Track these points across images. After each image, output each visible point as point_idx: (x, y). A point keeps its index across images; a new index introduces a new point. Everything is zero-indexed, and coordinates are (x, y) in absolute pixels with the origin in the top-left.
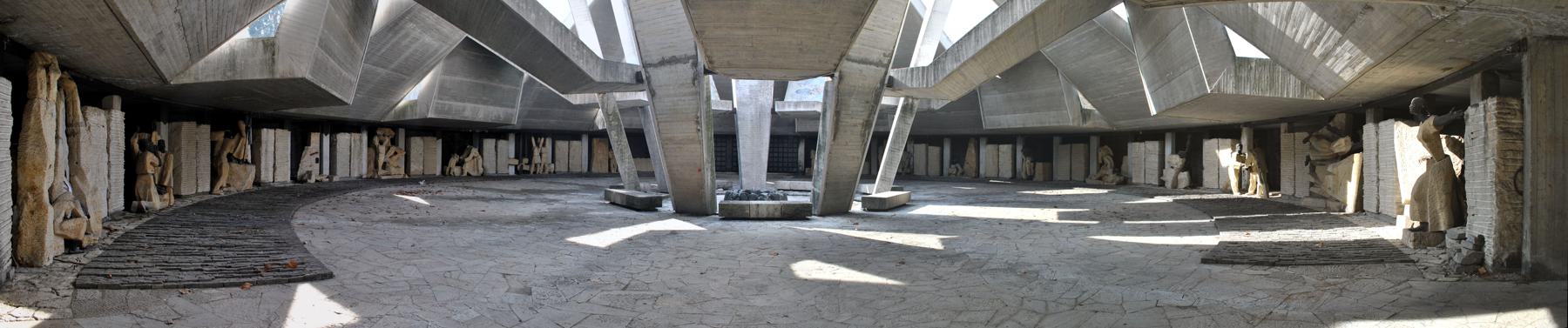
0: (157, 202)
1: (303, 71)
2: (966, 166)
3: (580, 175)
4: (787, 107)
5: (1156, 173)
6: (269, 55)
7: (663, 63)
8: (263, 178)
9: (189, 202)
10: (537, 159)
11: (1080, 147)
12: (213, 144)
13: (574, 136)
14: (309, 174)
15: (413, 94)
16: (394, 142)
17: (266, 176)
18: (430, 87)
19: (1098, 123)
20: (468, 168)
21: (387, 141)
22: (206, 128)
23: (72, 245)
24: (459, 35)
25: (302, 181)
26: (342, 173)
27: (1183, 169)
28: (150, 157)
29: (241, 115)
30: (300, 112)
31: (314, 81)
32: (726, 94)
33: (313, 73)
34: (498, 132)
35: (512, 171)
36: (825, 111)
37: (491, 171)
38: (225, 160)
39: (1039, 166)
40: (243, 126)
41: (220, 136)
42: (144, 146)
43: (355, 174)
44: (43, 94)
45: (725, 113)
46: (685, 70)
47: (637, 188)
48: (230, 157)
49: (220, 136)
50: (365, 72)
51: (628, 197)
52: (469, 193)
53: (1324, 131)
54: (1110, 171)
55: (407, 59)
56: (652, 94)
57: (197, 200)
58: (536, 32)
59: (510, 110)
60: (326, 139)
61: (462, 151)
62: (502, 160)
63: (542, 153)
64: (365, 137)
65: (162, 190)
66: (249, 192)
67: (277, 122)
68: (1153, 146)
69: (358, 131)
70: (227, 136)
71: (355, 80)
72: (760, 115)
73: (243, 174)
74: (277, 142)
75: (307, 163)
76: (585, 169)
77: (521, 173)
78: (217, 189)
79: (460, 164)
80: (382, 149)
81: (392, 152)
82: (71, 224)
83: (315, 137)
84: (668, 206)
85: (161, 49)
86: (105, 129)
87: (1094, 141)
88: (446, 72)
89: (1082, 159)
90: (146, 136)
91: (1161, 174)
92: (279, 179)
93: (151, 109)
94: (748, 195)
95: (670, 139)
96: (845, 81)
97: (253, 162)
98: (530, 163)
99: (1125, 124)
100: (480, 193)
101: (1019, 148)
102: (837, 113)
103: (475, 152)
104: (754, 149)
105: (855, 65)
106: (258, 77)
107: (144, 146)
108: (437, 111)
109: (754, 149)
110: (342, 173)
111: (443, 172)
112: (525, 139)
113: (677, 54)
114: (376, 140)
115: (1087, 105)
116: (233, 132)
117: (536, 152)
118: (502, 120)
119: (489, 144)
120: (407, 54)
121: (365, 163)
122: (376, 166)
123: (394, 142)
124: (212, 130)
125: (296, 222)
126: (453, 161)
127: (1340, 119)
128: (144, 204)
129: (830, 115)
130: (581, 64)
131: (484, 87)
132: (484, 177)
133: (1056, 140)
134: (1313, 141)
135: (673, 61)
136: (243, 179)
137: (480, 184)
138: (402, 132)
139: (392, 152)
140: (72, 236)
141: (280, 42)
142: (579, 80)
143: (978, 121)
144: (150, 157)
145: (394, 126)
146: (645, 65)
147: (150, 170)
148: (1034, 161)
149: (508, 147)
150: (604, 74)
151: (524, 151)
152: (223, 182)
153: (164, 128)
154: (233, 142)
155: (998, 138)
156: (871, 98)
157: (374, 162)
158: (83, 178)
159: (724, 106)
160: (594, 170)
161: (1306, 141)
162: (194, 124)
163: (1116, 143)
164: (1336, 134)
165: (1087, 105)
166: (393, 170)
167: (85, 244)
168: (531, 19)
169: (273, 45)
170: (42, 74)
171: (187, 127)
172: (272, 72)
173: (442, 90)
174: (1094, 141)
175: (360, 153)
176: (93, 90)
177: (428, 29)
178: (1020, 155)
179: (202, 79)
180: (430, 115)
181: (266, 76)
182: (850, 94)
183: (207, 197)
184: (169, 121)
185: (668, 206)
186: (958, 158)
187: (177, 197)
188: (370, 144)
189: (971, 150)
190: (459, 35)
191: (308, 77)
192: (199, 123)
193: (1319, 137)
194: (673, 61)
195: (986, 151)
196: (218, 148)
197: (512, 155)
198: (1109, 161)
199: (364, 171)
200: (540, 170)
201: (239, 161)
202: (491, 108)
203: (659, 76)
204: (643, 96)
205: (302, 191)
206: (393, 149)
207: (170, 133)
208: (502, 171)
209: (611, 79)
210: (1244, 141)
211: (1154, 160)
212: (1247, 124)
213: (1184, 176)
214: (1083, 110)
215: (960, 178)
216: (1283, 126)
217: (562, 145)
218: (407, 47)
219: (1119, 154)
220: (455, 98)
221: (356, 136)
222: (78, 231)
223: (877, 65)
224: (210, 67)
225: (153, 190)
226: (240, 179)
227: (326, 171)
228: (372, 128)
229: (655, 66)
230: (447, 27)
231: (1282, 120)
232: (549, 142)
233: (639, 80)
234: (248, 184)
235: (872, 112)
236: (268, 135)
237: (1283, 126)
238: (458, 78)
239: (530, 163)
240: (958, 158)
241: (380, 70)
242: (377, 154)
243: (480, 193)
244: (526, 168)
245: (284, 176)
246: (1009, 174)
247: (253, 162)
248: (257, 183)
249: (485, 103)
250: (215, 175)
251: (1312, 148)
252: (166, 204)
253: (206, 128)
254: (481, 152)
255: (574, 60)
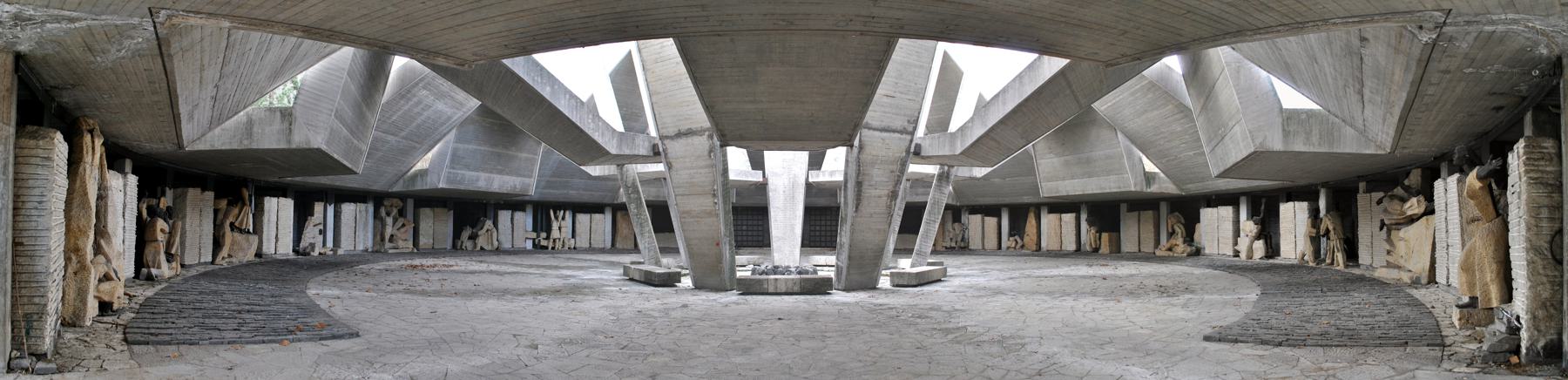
0: (165, 270)
1: (318, 141)
2: (1026, 239)
3: (603, 251)
4: (818, 177)
5: (1231, 241)
6: (286, 124)
7: (679, 135)
8: (265, 249)
9: (193, 272)
10: (555, 233)
11: (1148, 215)
12: (216, 212)
13: (595, 208)
14: (313, 246)
15: (422, 164)
16: (402, 213)
17: (268, 248)
18: (441, 154)
19: (1165, 186)
20: (481, 242)
21: (395, 211)
22: (210, 195)
23: (105, 307)
24: (474, 103)
25: (305, 254)
26: (346, 246)
27: (1258, 237)
28: (161, 224)
29: (244, 182)
30: (310, 182)
31: (329, 151)
32: (757, 163)
33: (328, 143)
34: (515, 204)
35: (529, 245)
36: (846, 181)
37: (507, 245)
38: (227, 229)
39: (1105, 236)
40: (246, 194)
41: (223, 204)
42: (153, 212)
43: (360, 247)
44: (88, 158)
45: (756, 184)
46: (702, 143)
47: (658, 263)
48: (232, 225)
49: (223, 204)
50: (375, 139)
51: (648, 273)
52: (483, 267)
53: (1399, 191)
54: (1180, 241)
55: (419, 126)
56: (669, 166)
57: (202, 269)
58: (551, 105)
59: (527, 180)
60: (331, 210)
61: (476, 223)
62: (519, 233)
63: (561, 226)
64: (371, 207)
65: (170, 257)
66: (249, 264)
67: (280, 191)
68: (1226, 212)
69: (364, 202)
70: (229, 204)
71: (365, 148)
72: (794, 186)
73: (245, 245)
74: (280, 211)
75: (311, 234)
76: (609, 245)
77: (538, 248)
78: (219, 260)
79: (473, 237)
80: (389, 221)
81: (399, 224)
82: (106, 286)
83: (318, 207)
84: (687, 282)
85: (191, 117)
86: (123, 189)
87: (1164, 208)
88: (458, 140)
89: (1151, 228)
90: (154, 202)
91: (1236, 243)
92: (281, 251)
93: (164, 176)
94: (775, 270)
95: (687, 212)
96: (867, 150)
97: (255, 232)
98: (548, 238)
99: (1194, 188)
100: (493, 267)
101: (1084, 217)
102: (859, 184)
103: (489, 224)
104: (786, 222)
105: (877, 133)
106: (275, 146)
107: (153, 212)
108: (449, 181)
109: (786, 222)
110: (346, 246)
111: (454, 246)
112: (543, 212)
113: (694, 127)
114: (383, 212)
115: (1150, 166)
116: (237, 201)
117: (555, 225)
118: (518, 191)
119: (504, 216)
120: (419, 121)
121: (370, 235)
122: (383, 239)
123: (402, 213)
124: (217, 197)
125: (311, 292)
126: (466, 234)
127: (1415, 178)
128: (154, 271)
129: (851, 185)
130: (596, 137)
131: (499, 155)
132: (498, 251)
133: (1124, 207)
134: (1385, 203)
135: (689, 133)
136: (241, 250)
137: (495, 258)
138: (410, 203)
139: (399, 224)
140: (106, 299)
141: (298, 113)
142: (596, 152)
143: (1035, 189)
144: (161, 224)
145: (403, 196)
146: (662, 138)
147: (160, 237)
148: (1100, 231)
149: (525, 220)
150: (620, 146)
151: (542, 224)
152: (224, 252)
153: (169, 193)
154: (236, 211)
155: (1059, 206)
156: (896, 167)
157: (379, 235)
158: (109, 241)
159: (756, 177)
160: (618, 245)
161: (1379, 202)
162: (198, 191)
163: (1185, 210)
164: (1411, 192)
165: (1150, 166)
166: (401, 244)
167: (115, 307)
168: (546, 92)
169: (291, 115)
170: (88, 138)
171: (193, 193)
172: (289, 142)
173: (456, 159)
174: (1164, 208)
175: (366, 224)
176: (116, 157)
177: (441, 96)
178: (1084, 226)
179: (218, 146)
180: (441, 185)
181: (283, 146)
182: (873, 164)
183: (211, 267)
184: (174, 187)
185: (687, 282)
186: (1017, 229)
187: (183, 266)
188: (376, 215)
189: (1031, 221)
190: (474, 103)
191: (324, 147)
192: (204, 190)
193: (1393, 197)
194: (689, 133)
195: (1048, 220)
196: (220, 216)
197: (530, 227)
198: (1179, 230)
199: (370, 244)
200: (559, 245)
201: (241, 231)
202: (507, 178)
203: (675, 148)
204: (660, 167)
205: (304, 264)
206: (401, 221)
207: (175, 199)
208: (519, 244)
209: (627, 152)
210: (1322, 204)
211: (1228, 227)
212: (1324, 185)
213: (1259, 245)
214: (1145, 173)
215: (1020, 251)
216: (1362, 185)
217: (583, 219)
218: (419, 114)
219: (1191, 223)
220: (467, 167)
221: (361, 206)
222: (112, 294)
223: (901, 132)
224: (221, 138)
225: (163, 257)
226: (242, 249)
227: (330, 244)
228: (377, 199)
229: (671, 138)
230: (461, 95)
231: (1361, 178)
232: (568, 215)
233: (656, 154)
234: (250, 256)
235: (898, 182)
236: (271, 203)
237: (1362, 185)
238: (471, 147)
239: (548, 238)
240: (1017, 229)
241: (390, 138)
242: (384, 225)
243: (493, 267)
244: (544, 243)
245: (286, 248)
246: (1072, 247)
247: (255, 232)
248: (259, 255)
249: (500, 172)
250: (217, 244)
251: (1385, 211)
252: (173, 273)
253: (210, 195)
254: (495, 224)
255: (589, 132)
